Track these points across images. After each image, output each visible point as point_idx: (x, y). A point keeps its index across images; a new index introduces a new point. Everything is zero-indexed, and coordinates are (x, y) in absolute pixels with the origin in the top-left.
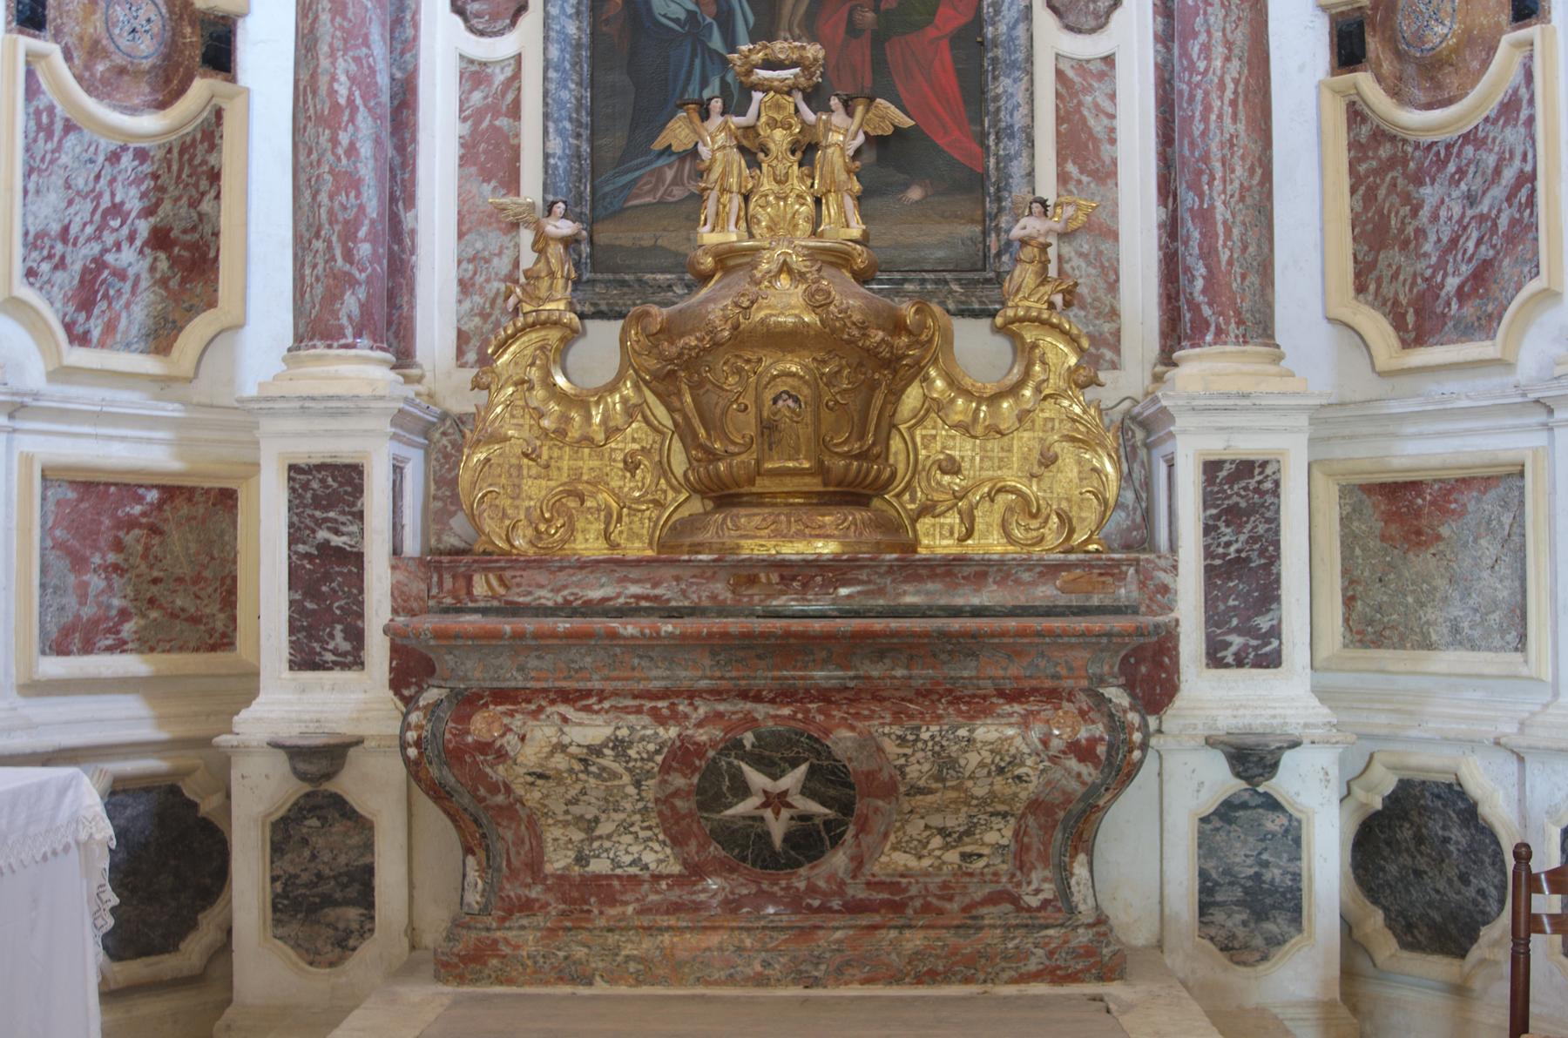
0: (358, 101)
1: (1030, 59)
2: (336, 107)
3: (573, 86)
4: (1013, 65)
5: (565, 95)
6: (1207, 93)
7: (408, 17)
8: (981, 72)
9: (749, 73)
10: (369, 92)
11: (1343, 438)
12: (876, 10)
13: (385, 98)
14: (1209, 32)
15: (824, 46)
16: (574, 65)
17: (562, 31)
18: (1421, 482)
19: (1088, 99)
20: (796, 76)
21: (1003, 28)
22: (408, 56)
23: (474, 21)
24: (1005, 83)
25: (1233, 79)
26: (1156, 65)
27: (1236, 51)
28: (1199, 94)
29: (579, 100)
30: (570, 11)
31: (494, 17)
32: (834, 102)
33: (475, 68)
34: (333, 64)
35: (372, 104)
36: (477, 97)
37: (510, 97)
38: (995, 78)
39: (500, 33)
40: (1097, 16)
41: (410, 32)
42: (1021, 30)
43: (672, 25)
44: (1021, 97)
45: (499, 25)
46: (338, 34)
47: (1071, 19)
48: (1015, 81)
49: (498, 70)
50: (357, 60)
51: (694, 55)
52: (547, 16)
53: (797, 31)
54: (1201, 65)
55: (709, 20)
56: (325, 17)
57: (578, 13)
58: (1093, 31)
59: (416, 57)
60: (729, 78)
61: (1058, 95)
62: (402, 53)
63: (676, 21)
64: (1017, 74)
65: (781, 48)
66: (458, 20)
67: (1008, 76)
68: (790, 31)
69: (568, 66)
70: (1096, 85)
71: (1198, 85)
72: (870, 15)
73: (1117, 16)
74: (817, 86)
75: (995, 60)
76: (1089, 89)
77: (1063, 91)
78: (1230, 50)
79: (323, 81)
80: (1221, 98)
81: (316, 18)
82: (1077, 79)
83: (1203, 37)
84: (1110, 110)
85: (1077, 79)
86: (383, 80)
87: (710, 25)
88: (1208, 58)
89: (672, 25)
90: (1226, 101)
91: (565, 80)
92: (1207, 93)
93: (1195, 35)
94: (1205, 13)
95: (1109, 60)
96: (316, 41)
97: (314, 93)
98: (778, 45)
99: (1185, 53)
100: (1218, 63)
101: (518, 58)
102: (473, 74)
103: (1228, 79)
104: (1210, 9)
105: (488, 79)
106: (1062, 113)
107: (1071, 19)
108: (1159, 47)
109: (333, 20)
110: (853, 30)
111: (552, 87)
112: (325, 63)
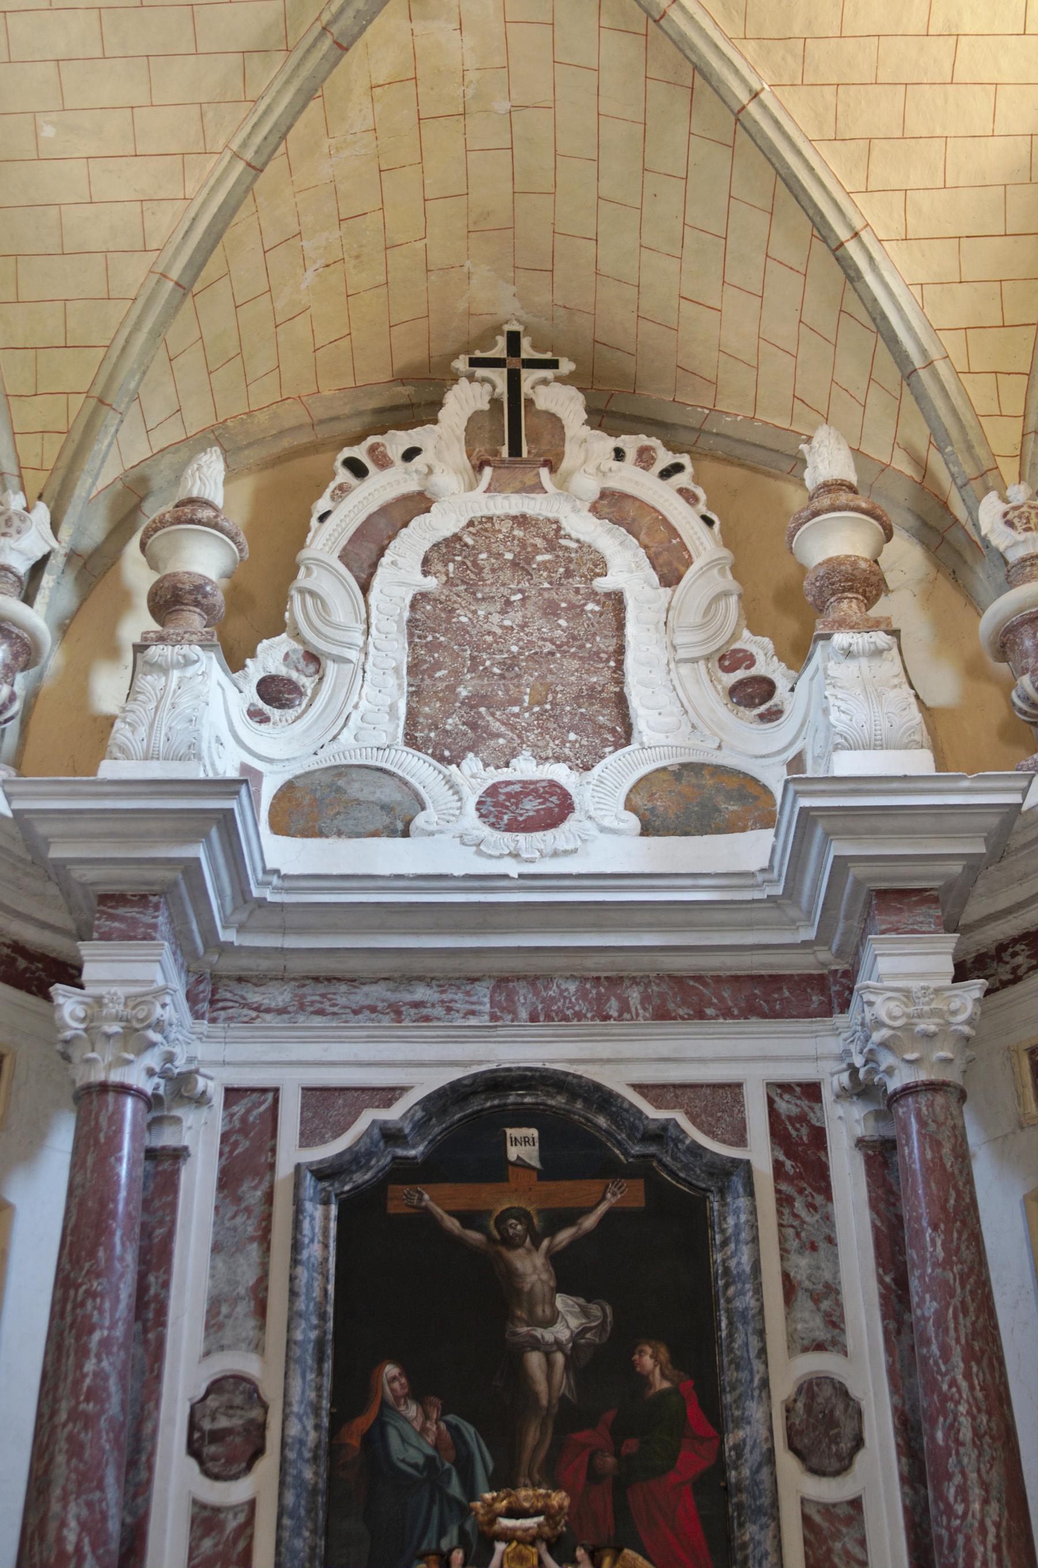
0: (87, 1549)
1: (775, 1504)
2: (62, 1555)
3: (307, 1534)
4: (759, 1511)
5: (298, 1544)
6: (968, 1539)
7: (144, 1459)
8: (729, 1519)
9: (492, 1522)
10: (99, 1538)
11: (892, 832)
12: (617, 1454)
13: (114, 1545)
14: (963, 1473)
15: (569, 1493)
16: (309, 1512)
17: (299, 1476)
18: (826, 1191)
19: (838, 1545)
20: (539, 1525)
21: (746, 1472)
22: (140, 1500)
23: (210, 1465)
24: (751, 1531)
25: (994, 1523)
26: (906, 1509)
27: (994, 1493)
28: (960, 1540)
29: (313, 1549)
30: (307, 1455)
31: (230, 1460)
32: (580, 1553)
33: (207, 1513)
34: (65, 1507)
35: (101, 1551)
36: (207, 1544)
37: (241, 1545)
38: (741, 1525)
39: (235, 1477)
40: (840, 1457)
41: (144, 1475)
42: (764, 1474)
43: (410, 1470)
44: (769, 1545)
45: (234, 1469)
46: (73, 1476)
47: (814, 1461)
48: (762, 1528)
49: (230, 1516)
50: (90, 1505)
51: (432, 1501)
52: (283, 1461)
53: (537, 1477)
54: (960, 1509)
55: (447, 1465)
56: (61, 1459)
57: (315, 1458)
58: (837, 1473)
59: (148, 1501)
60: (468, 1526)
61: (806, 1542)
62: (135, 1497)
63: (415, 1466)
64: (764, 1520)
65: (525, 1495)
66: (193, 1464)
67: (755, 1523)
68: (530, 1476)
69: (302, 1512)
70: (844, 1530)
71: (958, 1530)
72: (610, 1460)
73: (860, 1458)
74: (560, 1537)
75: (740, 1506)
76: (837, 1535)
77: (811, 1537)
78: (987, 1491)
79: (52, 1526)
80: (984, 1543)
81: (52, 1459)
82: (825, 1525)
83: (958, 1479)
84: (861, 1557)
85: (825, 1525)
86: (113, 1526)
87: (449, 1471)
88: (966, 1500)
89: (410, 1470)
90: (990, 1547)
91: (300, 1528)
92: (968, 1539)
93: (949, 1477)
94: (957, 1453)
95: (856, 1504)
96: (49, 1484)
97: (42, 1538)
98: (523, 1493)
99: (941, 1496)
100: (976, 1506)
101: (252, 1504)
102: (205, 1519)
103: (989, 1523)
104: (962, 1450)
105: (220, 1526)
106: (812, 1561)
107: (814, 1461)
108: (907, 1489)
109: (68, 1462)
110: (593, 1476)
111: (286, 1534)
112: (56, 1507)
